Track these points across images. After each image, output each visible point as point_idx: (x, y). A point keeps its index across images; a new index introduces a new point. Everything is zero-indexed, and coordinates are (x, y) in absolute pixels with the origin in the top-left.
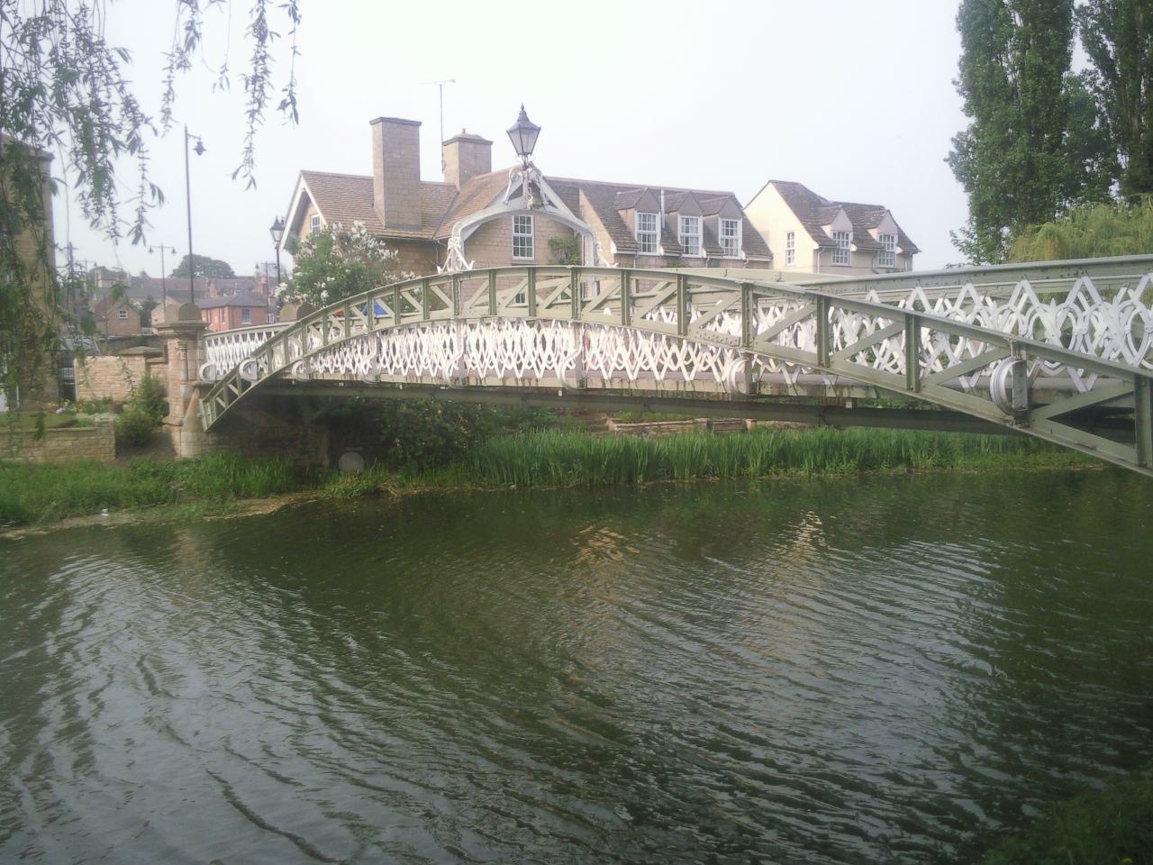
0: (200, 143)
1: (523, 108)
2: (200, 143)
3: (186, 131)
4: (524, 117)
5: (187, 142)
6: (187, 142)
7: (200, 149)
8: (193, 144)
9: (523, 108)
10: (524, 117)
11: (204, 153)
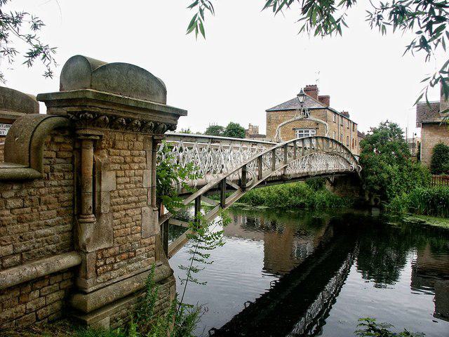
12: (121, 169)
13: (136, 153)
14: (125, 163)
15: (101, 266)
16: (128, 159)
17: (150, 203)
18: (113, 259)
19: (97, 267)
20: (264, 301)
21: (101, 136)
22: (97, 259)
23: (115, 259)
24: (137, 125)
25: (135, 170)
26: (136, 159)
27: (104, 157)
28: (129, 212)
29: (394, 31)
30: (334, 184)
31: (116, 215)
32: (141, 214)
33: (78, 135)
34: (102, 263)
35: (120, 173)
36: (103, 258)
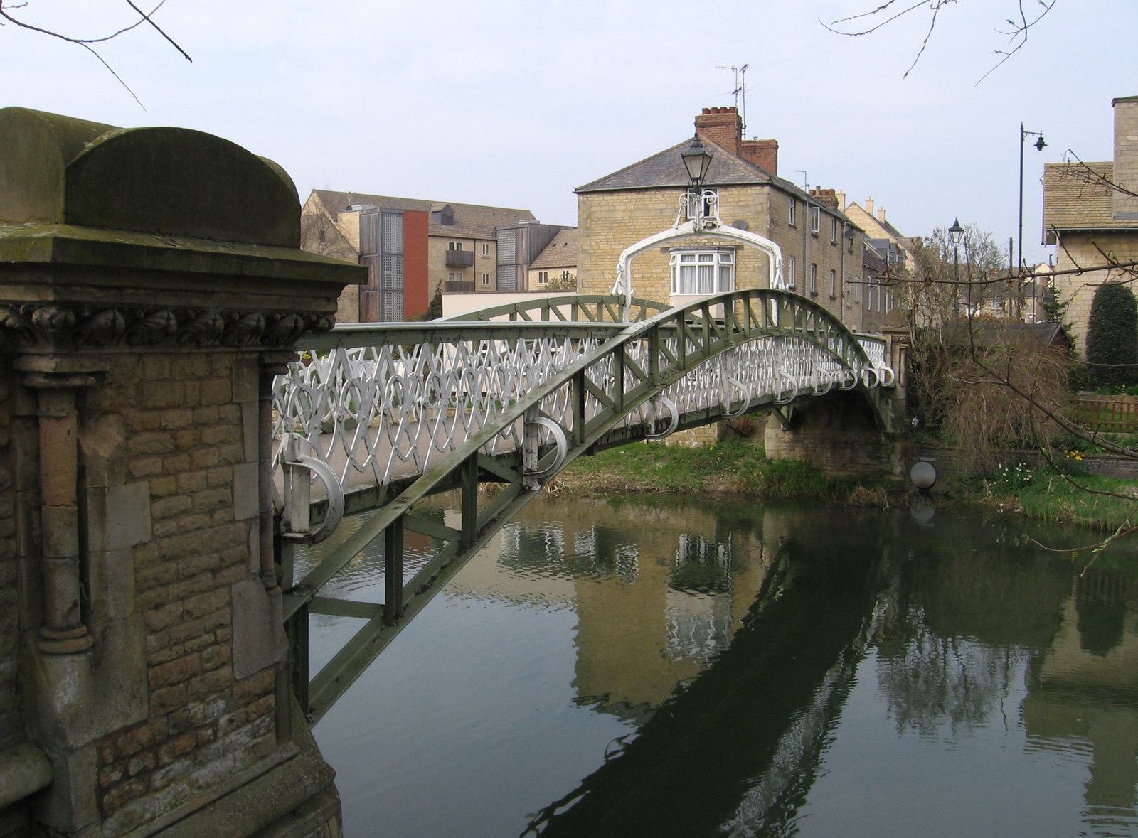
0: (1041, 139)
1: (957, 219)
2: (1041, 139)
3: (1022, 129)
4: (957, 224)
5: (1022, 140)
6: (1022, 140)
7: (1040, 145)
8: (1031, 141)
9: (957, 219)
10: (957, 224)
11: (1044, 148)
12: (166, 473)
13: (209, 413)
14: (178, 450)
15: (118, 783)
16: (187, 438)
17: (255, 564)
18: (149, 761)
19: (102, 790)
20: (605, 784)
21: (100, 375)
22: (102, 764)
23: (157, 759)
24: (165, 330)
25: (207, 468)
26: (209, 435)
27: (105, 442)
28: (191, 604)
29: (1022, 126)
30: (794, 424)
31: (157, 618)
32: (230, 604)
33: (25, 374)
34: (116, 776)
35: (162, 486)
36: (120, 759)
